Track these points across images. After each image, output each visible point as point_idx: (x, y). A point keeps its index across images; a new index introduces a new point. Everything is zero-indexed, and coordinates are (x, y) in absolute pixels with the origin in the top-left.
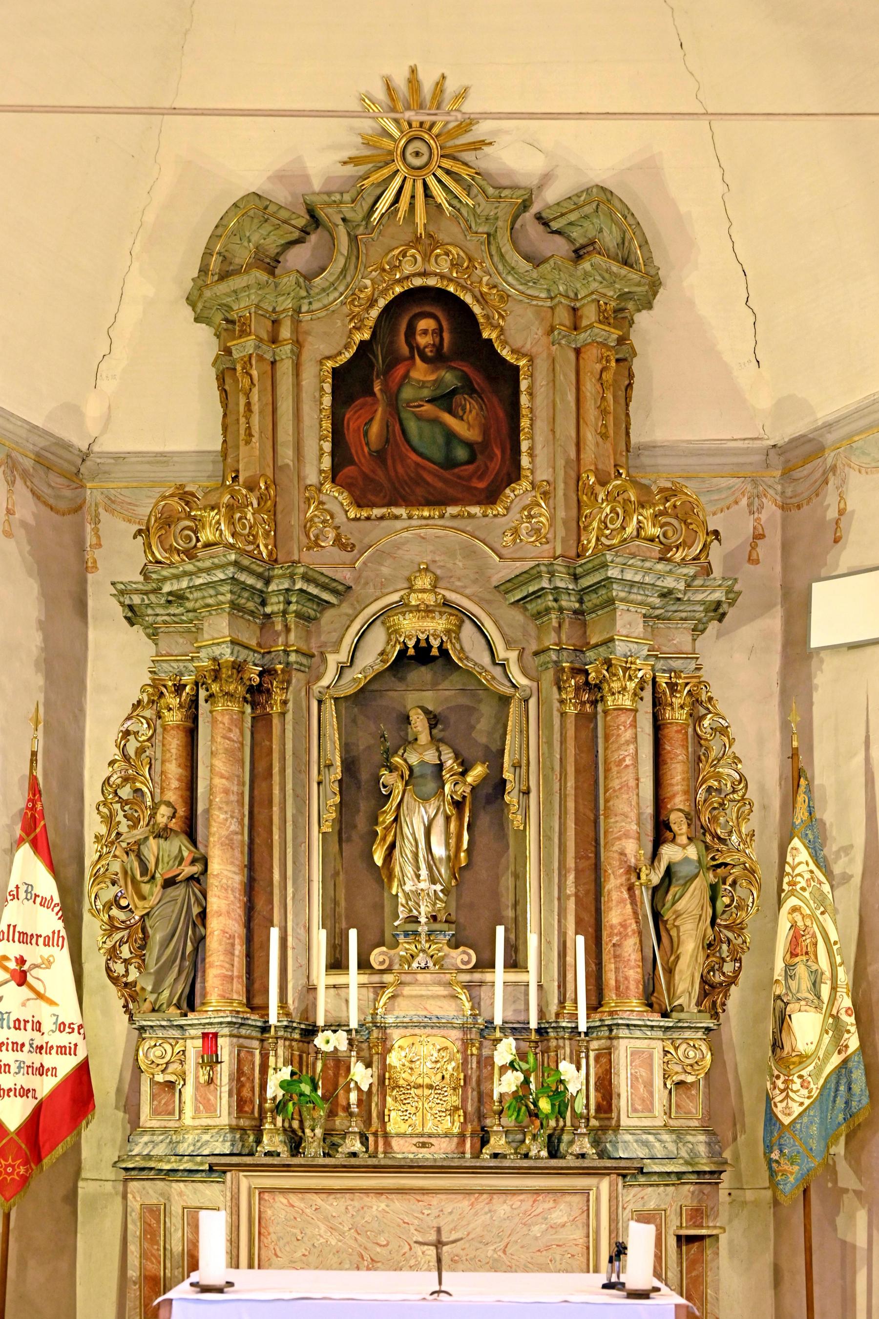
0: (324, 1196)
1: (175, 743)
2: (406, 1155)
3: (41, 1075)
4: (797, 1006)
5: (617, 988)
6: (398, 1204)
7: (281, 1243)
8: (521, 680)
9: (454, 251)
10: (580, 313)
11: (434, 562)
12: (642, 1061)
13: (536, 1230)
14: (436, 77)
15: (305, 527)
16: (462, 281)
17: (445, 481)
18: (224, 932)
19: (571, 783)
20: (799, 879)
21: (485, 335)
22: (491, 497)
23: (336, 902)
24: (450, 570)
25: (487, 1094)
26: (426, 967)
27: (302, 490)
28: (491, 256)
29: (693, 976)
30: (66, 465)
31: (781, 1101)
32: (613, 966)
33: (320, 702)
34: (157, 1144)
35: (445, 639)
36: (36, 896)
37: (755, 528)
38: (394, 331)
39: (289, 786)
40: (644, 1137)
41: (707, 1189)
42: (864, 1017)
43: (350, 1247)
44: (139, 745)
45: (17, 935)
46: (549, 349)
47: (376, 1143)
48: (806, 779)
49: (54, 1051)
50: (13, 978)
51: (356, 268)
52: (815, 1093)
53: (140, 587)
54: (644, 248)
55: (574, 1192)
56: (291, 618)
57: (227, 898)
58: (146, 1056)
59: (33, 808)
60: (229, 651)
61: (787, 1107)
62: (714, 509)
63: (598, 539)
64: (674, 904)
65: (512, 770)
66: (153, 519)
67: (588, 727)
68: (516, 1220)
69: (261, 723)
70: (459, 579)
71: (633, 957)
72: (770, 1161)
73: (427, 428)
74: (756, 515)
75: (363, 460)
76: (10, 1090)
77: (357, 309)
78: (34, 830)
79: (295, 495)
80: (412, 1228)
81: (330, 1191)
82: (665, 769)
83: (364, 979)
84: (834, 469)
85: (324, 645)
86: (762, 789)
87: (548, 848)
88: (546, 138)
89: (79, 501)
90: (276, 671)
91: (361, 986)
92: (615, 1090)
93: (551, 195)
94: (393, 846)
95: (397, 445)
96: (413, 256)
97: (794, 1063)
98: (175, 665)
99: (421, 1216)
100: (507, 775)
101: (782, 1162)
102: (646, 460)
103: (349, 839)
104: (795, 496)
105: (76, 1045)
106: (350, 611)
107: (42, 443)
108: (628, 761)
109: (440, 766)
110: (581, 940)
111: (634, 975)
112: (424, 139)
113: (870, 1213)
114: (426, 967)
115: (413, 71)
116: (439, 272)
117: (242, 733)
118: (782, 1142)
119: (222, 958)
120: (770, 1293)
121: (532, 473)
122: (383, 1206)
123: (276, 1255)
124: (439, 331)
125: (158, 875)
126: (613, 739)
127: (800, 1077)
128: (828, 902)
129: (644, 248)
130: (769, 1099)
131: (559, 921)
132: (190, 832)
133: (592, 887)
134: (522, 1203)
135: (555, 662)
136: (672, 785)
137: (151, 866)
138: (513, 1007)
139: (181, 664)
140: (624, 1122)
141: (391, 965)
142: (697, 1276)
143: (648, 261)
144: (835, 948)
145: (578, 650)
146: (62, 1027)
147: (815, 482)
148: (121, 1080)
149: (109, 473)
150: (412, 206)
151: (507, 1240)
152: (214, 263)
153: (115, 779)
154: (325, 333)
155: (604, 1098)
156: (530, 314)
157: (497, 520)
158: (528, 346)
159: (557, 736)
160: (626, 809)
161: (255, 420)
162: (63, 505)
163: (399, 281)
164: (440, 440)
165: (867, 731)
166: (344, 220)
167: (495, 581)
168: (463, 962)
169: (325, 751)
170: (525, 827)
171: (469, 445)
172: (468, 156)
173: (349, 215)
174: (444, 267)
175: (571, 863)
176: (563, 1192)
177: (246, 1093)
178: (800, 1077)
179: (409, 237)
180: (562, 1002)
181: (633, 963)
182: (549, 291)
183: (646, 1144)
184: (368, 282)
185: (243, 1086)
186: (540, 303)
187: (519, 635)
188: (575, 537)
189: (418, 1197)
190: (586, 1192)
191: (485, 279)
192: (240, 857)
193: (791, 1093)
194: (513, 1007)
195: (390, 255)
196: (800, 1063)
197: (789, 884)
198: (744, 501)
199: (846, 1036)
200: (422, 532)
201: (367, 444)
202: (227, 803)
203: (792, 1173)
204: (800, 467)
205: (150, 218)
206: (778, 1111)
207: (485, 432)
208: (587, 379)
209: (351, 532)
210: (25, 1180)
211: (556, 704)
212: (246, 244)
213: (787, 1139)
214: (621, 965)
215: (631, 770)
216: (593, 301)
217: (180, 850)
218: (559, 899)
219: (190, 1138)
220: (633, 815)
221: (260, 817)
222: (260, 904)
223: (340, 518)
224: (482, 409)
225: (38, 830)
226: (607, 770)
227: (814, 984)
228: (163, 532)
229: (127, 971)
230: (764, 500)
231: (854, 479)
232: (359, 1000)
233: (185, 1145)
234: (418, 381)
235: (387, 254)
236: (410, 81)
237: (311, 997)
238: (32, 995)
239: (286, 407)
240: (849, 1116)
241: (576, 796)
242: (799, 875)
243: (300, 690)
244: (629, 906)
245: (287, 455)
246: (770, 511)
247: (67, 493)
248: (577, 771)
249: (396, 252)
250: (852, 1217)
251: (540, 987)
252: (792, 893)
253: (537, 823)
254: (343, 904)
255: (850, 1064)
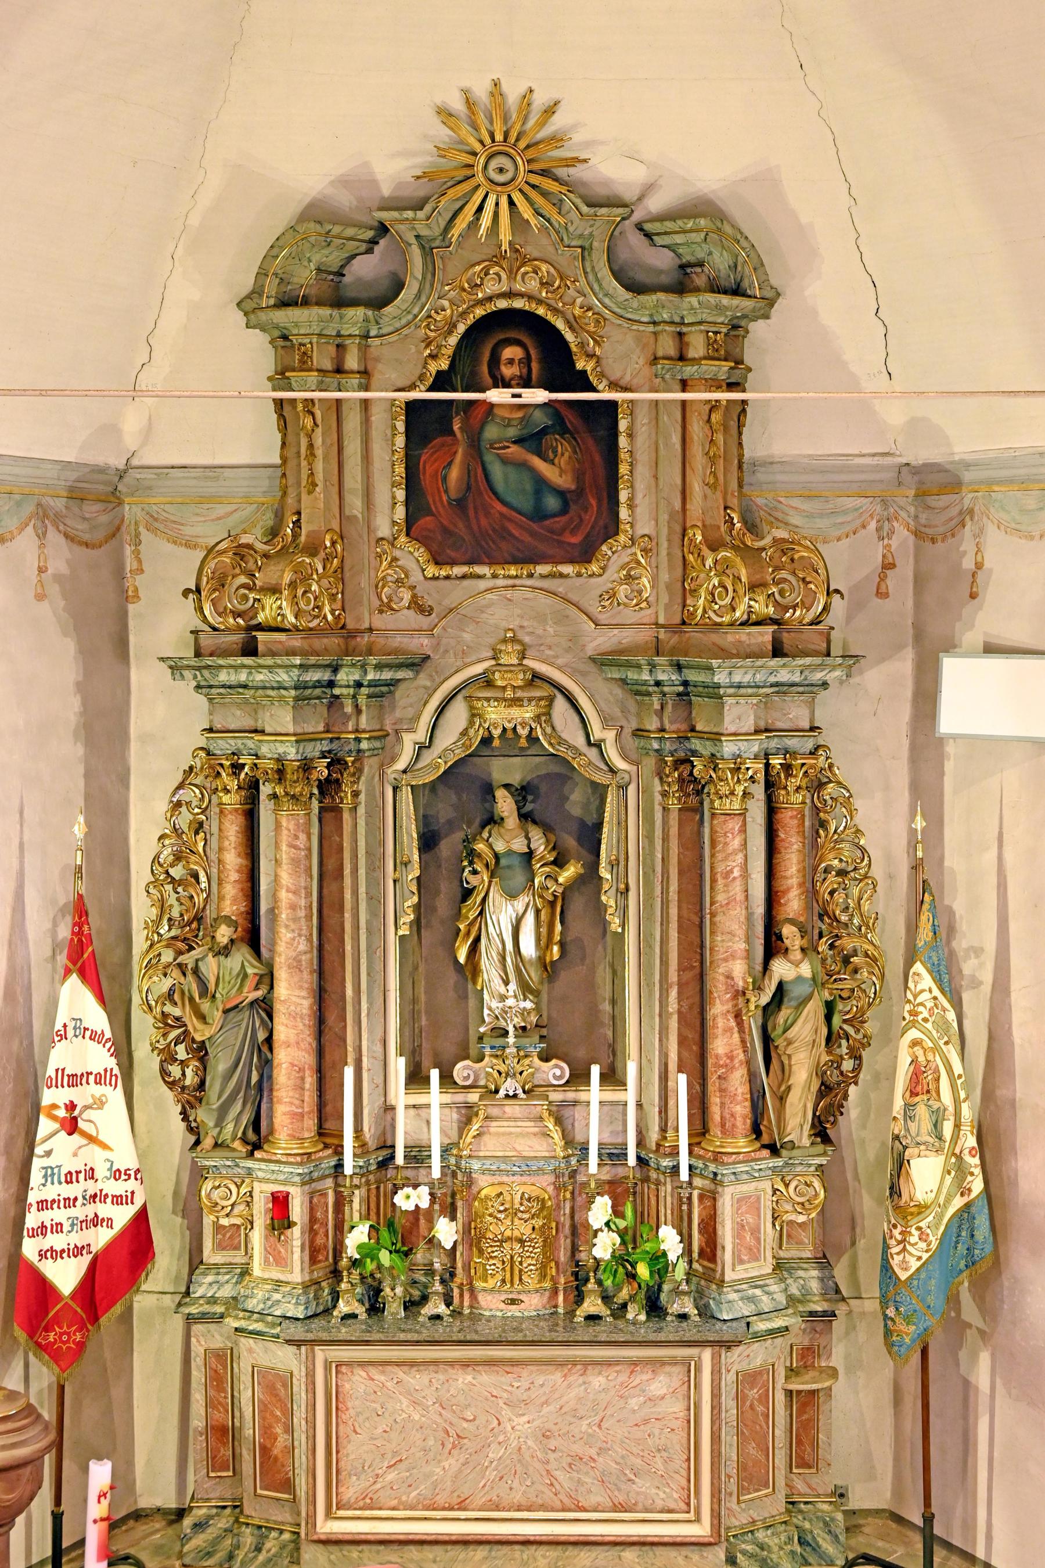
0: (406, 1368)
1: (233, 829)
2: (493, 1313)
3: (95, 1226)
4: (916, 1151)
5: (723, 1125)
6: (486, 1378)
7: (361, 1419)
8: (620, 764)
9: (544, 267)
10: (686, 339)
11: (521, 627)
12: (752, 1199)
13: (634, 1403)
14: (522, 89)
15: (377, 587)
16: (552, 302)
17: (533, 534)
18: (293, 1065)
19: (674, 887)
20: (921, 1009)
21: (580, 365)
22: (585, 554)
23: (414, 1001)
24: (540, 637)
25: (582, 1225)
26: (515, 1096)
27: (373, 543)
28: (585, 273)
29: (805, 1106)
30: (101, 487)
31: (898, 1254)
32: (718, 1100)
33: (395, 789)
34: (222, 1285)
35: (533, 725)
36: (85, 1029)
37: (884, 556)
38: (476, 361)
39: (362, 890)
40: (750, 1292)
41: (819, 1327)
42: (989, 1140)
43: (435, 1423)
44: (191, 817)
45: (66, 1079)
46: (650, 380)
47: (461, 1296)
48: (932, 894)
49: (109, 1200)
50: (63, 1127)
51: (432, 285)
52: (934, 1245)
53: (192, 663)
54: (760, 271)
55: (674, 1362)
56: (362, 700)
57: (295, 1027)
58: (208, 1196)
59: (80, 933)
60: (294, 750)
61: (904, 1261)
62: (838, 533)
63: (705, 611)
64: (785, 1032)
65: (609, 868)
66: (205, 579)
67: (693, 820)
68: (612, 1392)
69: (330, 812)
70: (550, 648)
71: (740, 1091)
72: (886, 1317)
73: (513, 474)
74: (886, 541)
75: (441, 510)
76: (63, 1251)
77: (432, 334)
78: (83, 960)
79: (366, 550)
80: (501, 1402)
81: (412, 1364)
82: (777, 859)
83: (447, 1098)
84: (971, 512)
85: (400, 720)
86: (888, 857)
87: (650, 918)
88: (647, 133)
89: (117, 522)
90: (346, 763)
91: (443, 1106)
92: (719, 1241)
93: (655, 204)
94: (477, 940)
95: (480, 494)
96: (497, 274)
97: (912, 1214)
98: (232, 742)
99: (510, 1388)
100: (604, 873)
101: (897, 1320)
102: (761, 476)
103: (429, 925)
104: (930, 527)
105: (133, 1193)
106: (428, 684)
107: (74, 476)
108: (736, 873)
109: (529, 855)
110: (682, 1079)
111: (742, 1109)
112: (508, 150)
113: (993, 1355)
114: (515, 1096)
115: (496, 84)
116: (526, 290)
117: (309, 838)
118: (898, 1299)
119: (291, 1094)
120: (889, 1411)
121: (632, 527)
122: (469, 1378)
123: (355, 1431)
124: (527, 360)
125: (218, 995)
126: (719, 847)
127: (919, 1229)
128: (952, 1031)
129: (759, 271)
130: (886, 1247)
131: (660, 1040)
132: (253, 939)
133: (697, 999)
134: (618, 1377)
135: (657, 751)
136: (786, 878)
137: (212, 986)
138: (610, 1129)
139: (239, 742)
140: (729, 1276)
141: (476, 1080)
142: (809, 1420)
143: (764, 283)
144: (959, 1082)
145: (683, 739)
146: (117, 1175)
147: (951, 519)
148: (178, 1183)
149: (150, 488)
150: (496, 215)
151: (602, 1414)
152: (271, 287)
153: (166, 855)
154: (396, 360)
155: (707, 1243)
156: (630, 340)
157: (593, 580)
158: (628, 378)
159: (658, 833)
160: (735, 927)
161: (319, 466)
162: (100, 535)
163: (481, 302)
164: (529, 487)
165: (1001, 828)
166: (417, 237)
167: (591, 649)
168: (555, 1077)
169: (402, 843)
170: (623, 929)
171: (561, 494)
172: (562, 172)
173: (424, 232)
174: (532, 285)
175: (673, 976)
176: (662, 1363)
177: (320, 1241)
178: (919, 1229)
179: (490, 251)
180: (664, 1130)
181: (739, 1098)
182: (651, 315)
183: (751, 1299)
184: (446, 303)
185: (316, 1234)
186: (642, 328)
187: (617, 711)
188: (680, 600)
189: (507, 1369)
190: (686, 1363)
191: (579, 301)
192: (309, 979)
193: (908, 1247)
194: (610, 1129)
195: (471, 272)
196: (919, 1213)
197: (910, 1012)
198: (873, 525)
199: (969, 1179)
200: (509, 594)
201: (446, 491)
202: (295, 920)
203: (907, 1334)
204: (933, 498)
205: (194, 220)
206: (896, 1262)
207: (579, 477)
208: (695, 419)
209: (430, 595)
210: (81, 1346)
211: (658, 798)
212: (306, 263)
213: (904, 1296)
214: (727, 1100)
215: (738, 882)
216: (701, 331)
217: (243, 966)
218: (660, 1015)
219: (260, 1295)
220: (741, 933)
221: (331, 921)
222: (331, 1018)
223: (416, 577)
224: (575, 452)
225: (85, 956)
226: (713, 881)
227: (935, 1126)
228: (217, 594)
229: (184, 1074)
230: (895, 524)
231: (993, 537)
232: (442, 1120)
233: (255, 1301)
234: (503, 419)
235: (467, 269)
236: (492, 94)
237: (389, 1118)
238: (84, 1141)
239: (353, 447)
240: (971, 1264)
241: (679, 901)
242: (921, 1004)
243: (373, 777)
244: (736, 1035)
245: (355, 505)
246: (902, 537)
247: (104, 518)
248: (681, 873)
249: (478, 268)
250: (974, 1357)
251: (639, 1105)
252: (913, 1024)
253: (636, 920)
254: (423, 998)
255: (973, 1209)
